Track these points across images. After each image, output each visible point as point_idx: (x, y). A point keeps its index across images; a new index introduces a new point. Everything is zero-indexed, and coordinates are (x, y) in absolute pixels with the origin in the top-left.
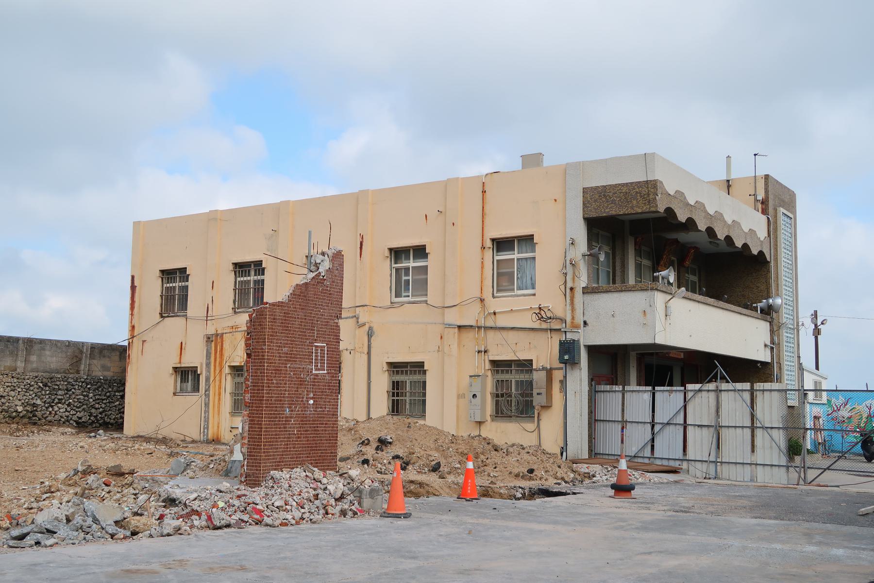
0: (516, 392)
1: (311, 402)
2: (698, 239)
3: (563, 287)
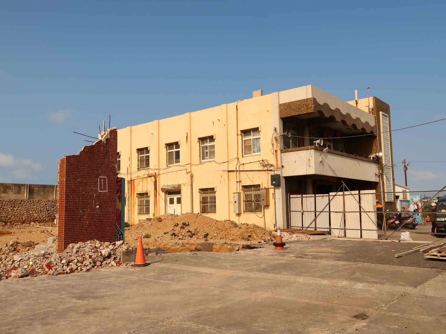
0: (254, 200)
1: (98, 207)
2: (339, 126)
3: (272, 150)
